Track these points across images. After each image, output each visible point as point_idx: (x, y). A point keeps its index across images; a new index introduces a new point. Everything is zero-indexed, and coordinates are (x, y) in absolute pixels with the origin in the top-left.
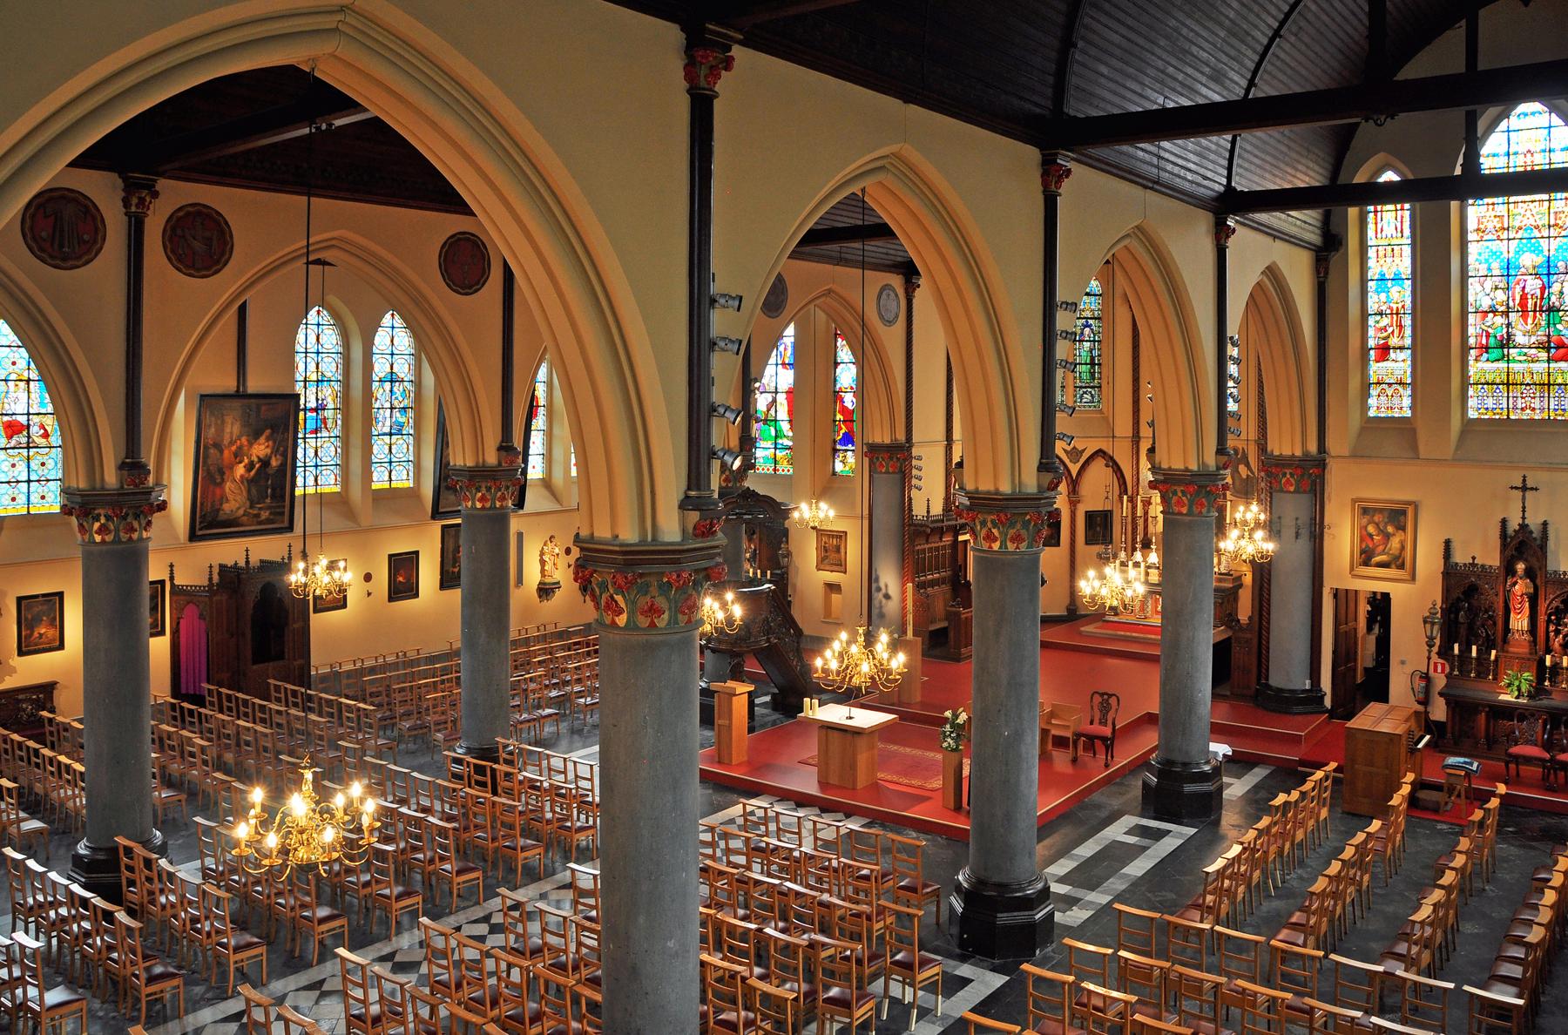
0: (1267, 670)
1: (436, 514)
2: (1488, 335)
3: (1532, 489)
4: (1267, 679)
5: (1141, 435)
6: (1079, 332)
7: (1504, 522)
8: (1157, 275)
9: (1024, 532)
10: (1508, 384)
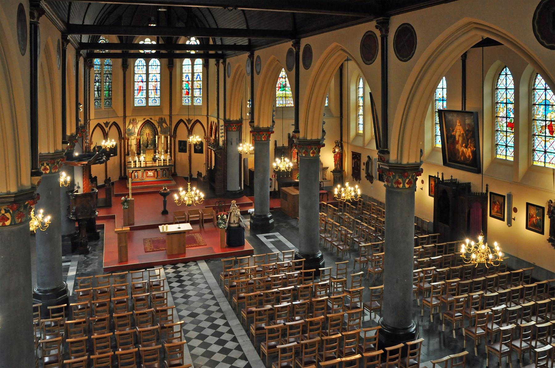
2: (281, 84)
3: (293, 125)
5: (126, 115)
7: (289, 134)
9: (315, 151)
10: (285, 97)
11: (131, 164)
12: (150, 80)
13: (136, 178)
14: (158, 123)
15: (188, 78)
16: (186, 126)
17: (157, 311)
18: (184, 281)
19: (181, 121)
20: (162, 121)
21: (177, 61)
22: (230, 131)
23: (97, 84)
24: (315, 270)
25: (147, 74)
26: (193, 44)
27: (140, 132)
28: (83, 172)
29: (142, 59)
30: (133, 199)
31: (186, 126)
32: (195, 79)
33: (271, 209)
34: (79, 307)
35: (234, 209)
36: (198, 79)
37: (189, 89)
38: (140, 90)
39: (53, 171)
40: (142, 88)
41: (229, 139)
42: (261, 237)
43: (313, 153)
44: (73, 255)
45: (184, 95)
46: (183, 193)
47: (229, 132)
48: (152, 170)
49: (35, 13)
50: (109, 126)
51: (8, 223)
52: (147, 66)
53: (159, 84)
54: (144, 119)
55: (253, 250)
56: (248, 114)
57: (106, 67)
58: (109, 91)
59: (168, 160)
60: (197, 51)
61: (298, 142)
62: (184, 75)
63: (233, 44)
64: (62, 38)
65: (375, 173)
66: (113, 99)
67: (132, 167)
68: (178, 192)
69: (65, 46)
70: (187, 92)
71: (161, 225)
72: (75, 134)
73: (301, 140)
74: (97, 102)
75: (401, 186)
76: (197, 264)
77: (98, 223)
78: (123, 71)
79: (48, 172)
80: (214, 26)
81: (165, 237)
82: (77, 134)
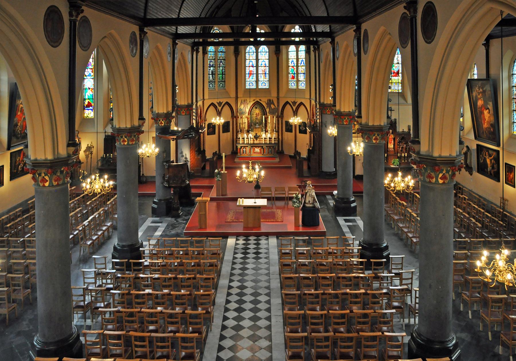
1: (9, 148)
4: (321, 169)
8: (68, 29)
9: (378, 137)
11: (240, 141)
13: (245, 153)
14: (267, 104)
16: (292, 108)
17: (319, 277)
18: (249, 253)
19: (287, 103)
21: (283, 48)
22: (324, 114)
23: (212, 68)
24: (366, 260)
25: (257, 60)
28: (191, 145)
29: (252, 47)
30: (226, 172)
31: (292, 108)
32: (299, 65)
33: (354, 193)
34: (176, 264)
35: (309, 189)
37: (294, 74)
38: (250, 74)
39: (130, 143)
41: (324, 121)
42: (341, 220)
43: (376, 139)
45: (290, 79)
46: (245, 170)
47: (323, 115)
48: (259, 147)
49: (73, 13)
50: (222, 106)
51: (47, 184)
52: (257, 52)
53: (267, 68)
54: (254, 100)
55: (325, 232)
56: (330, 98)
57: (220, 53)
58: (223, 74)
59: (273, 138)
60: (301, 38)
62: (290, 61)
65: (474, 164)
68: (240, 168)
70: (293, 76)
71: (241, 198)
72: (171, 111)
75: (434, 180)
76: (268, 239)
77: (193, 191)
78: (235, 57)
79: (126, 143)
82: (173, 112)
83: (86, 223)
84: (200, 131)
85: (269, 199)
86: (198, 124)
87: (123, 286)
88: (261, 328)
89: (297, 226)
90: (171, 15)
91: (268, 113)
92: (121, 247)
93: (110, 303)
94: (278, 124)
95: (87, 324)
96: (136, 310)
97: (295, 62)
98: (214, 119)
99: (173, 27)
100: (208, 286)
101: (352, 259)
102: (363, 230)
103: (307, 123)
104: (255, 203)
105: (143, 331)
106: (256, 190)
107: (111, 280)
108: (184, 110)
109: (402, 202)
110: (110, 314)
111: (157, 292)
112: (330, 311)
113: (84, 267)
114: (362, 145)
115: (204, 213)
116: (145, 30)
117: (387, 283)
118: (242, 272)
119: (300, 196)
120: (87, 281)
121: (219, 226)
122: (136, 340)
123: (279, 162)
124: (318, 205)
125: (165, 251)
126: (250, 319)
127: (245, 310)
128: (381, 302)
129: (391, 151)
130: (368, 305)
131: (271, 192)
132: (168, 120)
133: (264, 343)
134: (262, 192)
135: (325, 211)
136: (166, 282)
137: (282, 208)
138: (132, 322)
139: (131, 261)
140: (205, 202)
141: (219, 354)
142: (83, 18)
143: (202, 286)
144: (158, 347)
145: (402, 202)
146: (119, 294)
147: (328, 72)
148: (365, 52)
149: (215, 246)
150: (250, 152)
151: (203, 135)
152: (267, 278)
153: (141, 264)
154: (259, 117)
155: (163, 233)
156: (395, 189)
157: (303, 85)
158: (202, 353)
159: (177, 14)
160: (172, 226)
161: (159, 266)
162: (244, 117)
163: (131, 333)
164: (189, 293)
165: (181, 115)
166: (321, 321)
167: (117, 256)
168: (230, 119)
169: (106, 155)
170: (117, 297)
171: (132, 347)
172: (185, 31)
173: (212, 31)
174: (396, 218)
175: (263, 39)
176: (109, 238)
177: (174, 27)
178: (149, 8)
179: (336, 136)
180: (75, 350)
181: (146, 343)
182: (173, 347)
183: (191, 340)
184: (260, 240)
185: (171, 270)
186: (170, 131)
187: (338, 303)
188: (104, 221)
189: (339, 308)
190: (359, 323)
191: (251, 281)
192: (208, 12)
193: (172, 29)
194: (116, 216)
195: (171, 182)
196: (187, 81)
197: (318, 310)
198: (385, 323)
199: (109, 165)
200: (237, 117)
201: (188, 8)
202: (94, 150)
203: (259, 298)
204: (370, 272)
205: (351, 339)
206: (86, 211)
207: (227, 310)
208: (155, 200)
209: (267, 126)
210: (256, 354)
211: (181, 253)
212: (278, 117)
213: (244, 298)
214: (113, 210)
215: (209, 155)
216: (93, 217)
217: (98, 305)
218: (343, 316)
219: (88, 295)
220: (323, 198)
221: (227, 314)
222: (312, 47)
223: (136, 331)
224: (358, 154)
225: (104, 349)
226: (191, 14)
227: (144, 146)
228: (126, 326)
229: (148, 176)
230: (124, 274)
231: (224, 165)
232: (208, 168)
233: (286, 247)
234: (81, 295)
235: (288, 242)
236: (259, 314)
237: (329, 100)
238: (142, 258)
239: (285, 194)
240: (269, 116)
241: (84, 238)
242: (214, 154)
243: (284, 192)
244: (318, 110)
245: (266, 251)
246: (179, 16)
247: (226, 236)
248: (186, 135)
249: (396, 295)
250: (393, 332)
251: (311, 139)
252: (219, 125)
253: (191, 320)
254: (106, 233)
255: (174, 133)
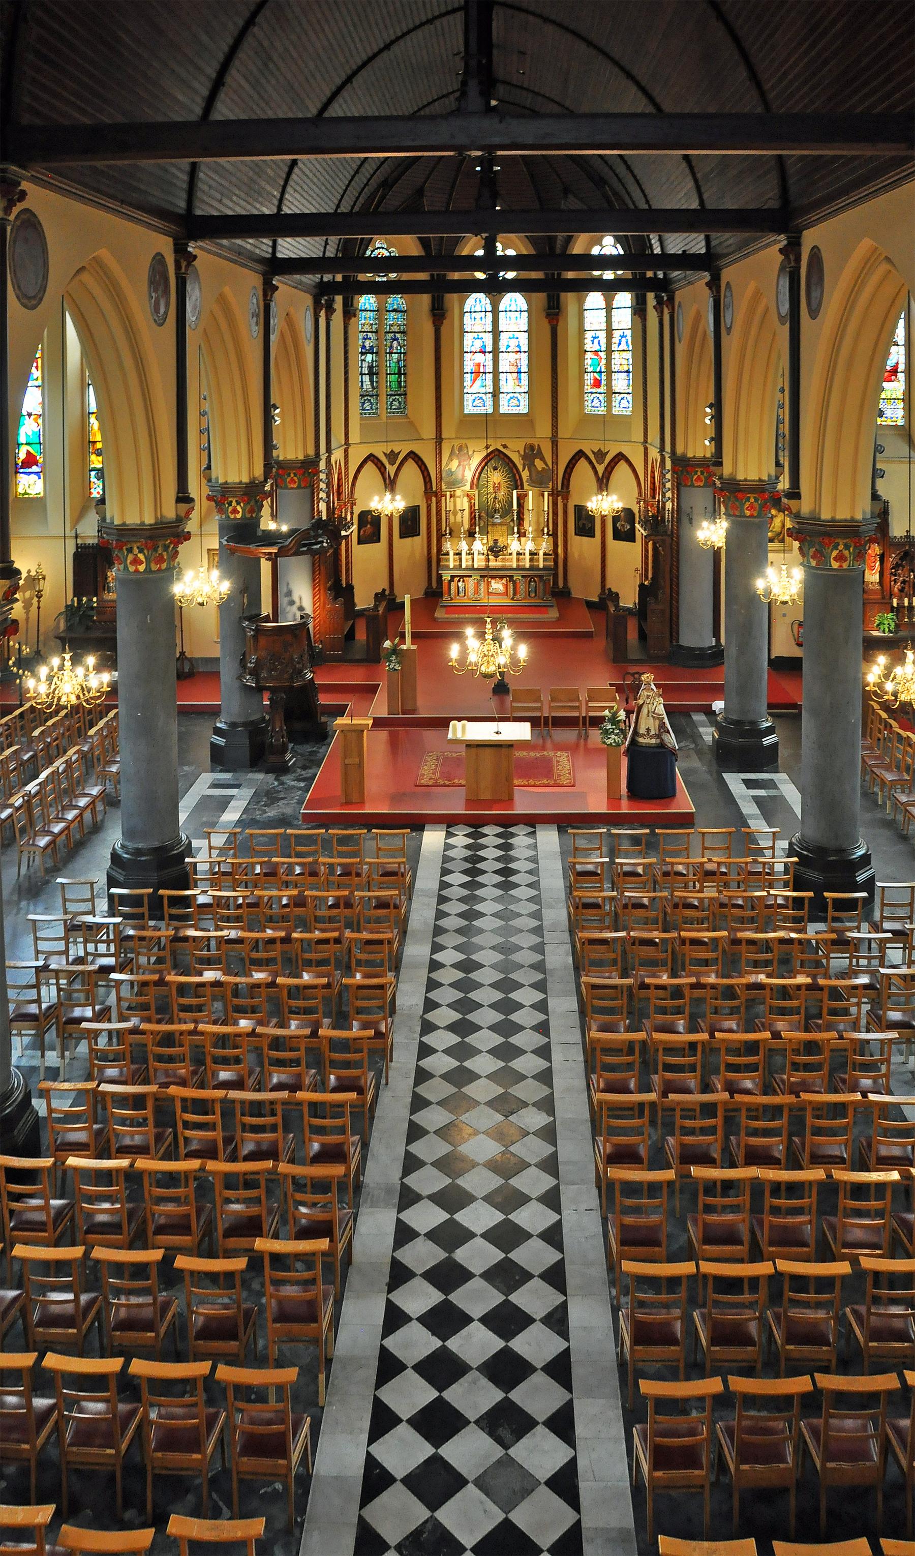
0: (678, 634)
6: (389, 344)
9: (846, 553)
11: (448, 560)
12: (502, 348)
13: (462, 594)
14: (524, 457)
15: (599, 344)
16: (594, 468)
17: (683, 941)
18: (484, 872)
19: (580, 454)
20: (531, 454)
22: (686, 486)
23: (369, 357)
24: (811, 894)
25: (496, 333)
26: (608, 253)
27: (478, 479)
28: (314, 573)
30: (414, 647)
31: (594, 468)
32: (615, 347)
33: (770, 706)
34: (284, 901)
35: (648, 697)
36: (623, 346)
37: (600, 372)
38: (477, 373)
39: (154, 567)
40: (482, 368)
41: (685, 506)
42: (734, 781)
43: (840, 558)
44: (252, 772)
45: (588, 389)
47: (683, 489)
48: (501, 577)
52: (495, 312)
53: (524, 357)
55: (692, 813)
56: (707, 443)
57: (392, 314)
58: (399, 374)
59: (541, 553)
61: (797, 526)
62: (589, 336)
63: (680, 252)
64: (176, 251)
66: (409, 396)
67: (451, 566)
68: (459, 636)
69: (183, 270)
70: (596, 379)
71: (459, 719)
72: (262, 479)
73: (804, 518)
74: (369, 401)
76: (534, 832)
77: (324, 700)
79: (142, 568)
80: (643, 206)
81: (463, 752)
82: (266, 481)
83: (32, 787)
84: (343, 533)
85: (535, 723)
86: (334, 513)
87: (143, 960)
88: (523, 1077)
89: (613, 798)
90: (258, 206)
91: (525, 484)
92: (131, 855)
93: (109, 1008)
94: (555, 514)
95: (47, 1064)
96: (184, 1027)
97: (603, 341)
98: (376, 498)
99: (265, 241)
100: (374, 961)
101: (772, 892)
102: (798, 811)
103: (636, 511)
104: (497, 733)
105: (202, 1086)
106: (496, 697)
107: (108, 945)
108: (295, 475)
109: (904, 734)
110: (110, 1038)
111: (238, 980)
112: (717, 1034)
113: (32, 908)
114: (798, 574)
115: (357, 761)
116: (190, 249)
117: (869, 958)
118: (467, 923)
119: (622, 715)
120: (43, 946)
121: (396, 798)
122: (185, 1110)
123: (559, 619)
124: (671, 740)
125: (253, 865)
126: (495, 1052)
127: (478, 1028)
128: (854, 1010)
129: (874, 592)
130: (820, 1016)
131: (539, 705)
132: (252, 503)
133: (535, 1119)
134: (514, 704)
135: (688, 756)
136: (257, 951)
137: (573, 749)
138: (171, 1059)
139: (161, 892)
140: (359, 731)
141: (412, 1148)
142: (24, 217)
143: (359, 963)
144: (245, 1128)
145: (904, 734)
146: (132, 983)
147: (699, 365)
148: (814, 313)
149: (392, 853)
150: (477, 592)
151: (347, 544)
152: (535, 940)
153: (187, 901)
154: (501, 494)
155: (244, 816)
156: (896, 697)
157: (624, 403)
158: (365, 1145)
159: (276, 202)
160: (270, 797)
161: (239, 906)
162: (458, 492)
163: (173, 1090)
164: (325, 981)
165: (287, 488)
166: (691, 1059)
167: (121, 878)
168: (421, 502)
169: (80, 601)
170: (125, 992)
171: (174, 1126)
172: (296, 251)
173: (368, 253)
174: (889, 777)
175: (511, 275)
176: (97, 828)
177: (268, 241)
178: (200, 185)
179: (719, 548)
180: (20, 1132)
181: (215, 1118)
182: (286, 1130)
183: (337, 1109)
184: (513, 835)
185: (271, 917)
186: (260, 534)
187: (733, 1011)
188: (82, 782)
189: (738, 1025)
190: (796, 1067)
191: (493, 948)
192: (357, 198)
193: (261, 246)
194: (114, 769)
195: (264, 674)
196: (300, 376)
197: (681, 1029)
198: (867, 1067)
199: (88, 628)
200: (439, 495)
201: (306, 188)
202: (46, 587)
203: (515, 996)
204: (821, 926)
205: (775, 1111)
206: (31, 753)
207: (428, 1027)
208: (219, 725)
209: (523, 520)
210: (512, 1149)
211: (298, 870)
212: (554, 494)
213: (474, 995)
214: (105, 751)
215: (363, 600)
216: (53, 772)
217: (77, 1012)
218: (752, 1048)
219: (48, 984)
220: (683, 721)
221: (431, 1039)
222: (651, 297)
223: (183, 1083)
224: (786, 598)
225: (99, 1132)
226: (314, 203)
227: (189, 575)
228: (156, 1070)
229: (197, 659)
230: (143, 928)
231: (408, 629)
232: (361, 635)
233: (587, 856)
234: (33, 987)
235: (590, 841)
236: (517, 1040)
237: (703, 447)
238: (192, 883)
239: (578, 708)
240: (530, 493)
241: (29, 829)
242: (379, 597)
243: (577, 704)
244: (669, 476)
245: (532, 866)
246: (279, 208)
247: (418, 824)
248: (304, 545)
249: (894, 990)
250: (890, 1093)
251: (647, 557)
252: (390, 518)
253: (336, 1056)
254: (88, 815)
255: (270, 538)
